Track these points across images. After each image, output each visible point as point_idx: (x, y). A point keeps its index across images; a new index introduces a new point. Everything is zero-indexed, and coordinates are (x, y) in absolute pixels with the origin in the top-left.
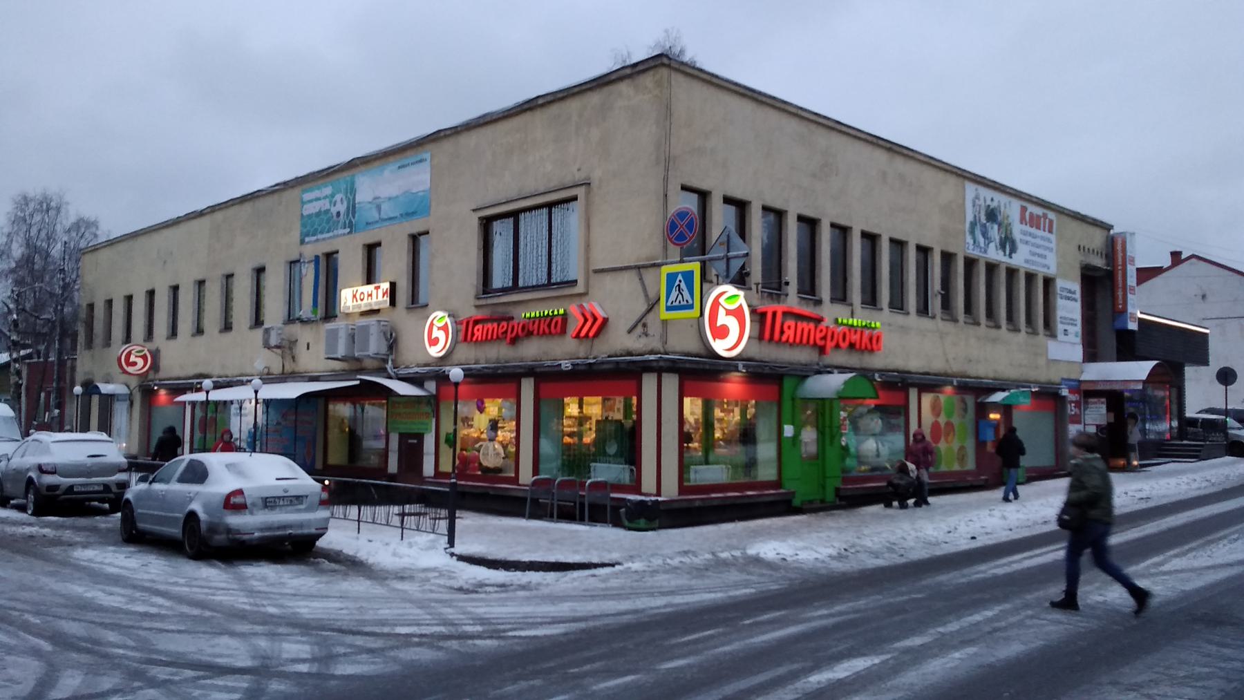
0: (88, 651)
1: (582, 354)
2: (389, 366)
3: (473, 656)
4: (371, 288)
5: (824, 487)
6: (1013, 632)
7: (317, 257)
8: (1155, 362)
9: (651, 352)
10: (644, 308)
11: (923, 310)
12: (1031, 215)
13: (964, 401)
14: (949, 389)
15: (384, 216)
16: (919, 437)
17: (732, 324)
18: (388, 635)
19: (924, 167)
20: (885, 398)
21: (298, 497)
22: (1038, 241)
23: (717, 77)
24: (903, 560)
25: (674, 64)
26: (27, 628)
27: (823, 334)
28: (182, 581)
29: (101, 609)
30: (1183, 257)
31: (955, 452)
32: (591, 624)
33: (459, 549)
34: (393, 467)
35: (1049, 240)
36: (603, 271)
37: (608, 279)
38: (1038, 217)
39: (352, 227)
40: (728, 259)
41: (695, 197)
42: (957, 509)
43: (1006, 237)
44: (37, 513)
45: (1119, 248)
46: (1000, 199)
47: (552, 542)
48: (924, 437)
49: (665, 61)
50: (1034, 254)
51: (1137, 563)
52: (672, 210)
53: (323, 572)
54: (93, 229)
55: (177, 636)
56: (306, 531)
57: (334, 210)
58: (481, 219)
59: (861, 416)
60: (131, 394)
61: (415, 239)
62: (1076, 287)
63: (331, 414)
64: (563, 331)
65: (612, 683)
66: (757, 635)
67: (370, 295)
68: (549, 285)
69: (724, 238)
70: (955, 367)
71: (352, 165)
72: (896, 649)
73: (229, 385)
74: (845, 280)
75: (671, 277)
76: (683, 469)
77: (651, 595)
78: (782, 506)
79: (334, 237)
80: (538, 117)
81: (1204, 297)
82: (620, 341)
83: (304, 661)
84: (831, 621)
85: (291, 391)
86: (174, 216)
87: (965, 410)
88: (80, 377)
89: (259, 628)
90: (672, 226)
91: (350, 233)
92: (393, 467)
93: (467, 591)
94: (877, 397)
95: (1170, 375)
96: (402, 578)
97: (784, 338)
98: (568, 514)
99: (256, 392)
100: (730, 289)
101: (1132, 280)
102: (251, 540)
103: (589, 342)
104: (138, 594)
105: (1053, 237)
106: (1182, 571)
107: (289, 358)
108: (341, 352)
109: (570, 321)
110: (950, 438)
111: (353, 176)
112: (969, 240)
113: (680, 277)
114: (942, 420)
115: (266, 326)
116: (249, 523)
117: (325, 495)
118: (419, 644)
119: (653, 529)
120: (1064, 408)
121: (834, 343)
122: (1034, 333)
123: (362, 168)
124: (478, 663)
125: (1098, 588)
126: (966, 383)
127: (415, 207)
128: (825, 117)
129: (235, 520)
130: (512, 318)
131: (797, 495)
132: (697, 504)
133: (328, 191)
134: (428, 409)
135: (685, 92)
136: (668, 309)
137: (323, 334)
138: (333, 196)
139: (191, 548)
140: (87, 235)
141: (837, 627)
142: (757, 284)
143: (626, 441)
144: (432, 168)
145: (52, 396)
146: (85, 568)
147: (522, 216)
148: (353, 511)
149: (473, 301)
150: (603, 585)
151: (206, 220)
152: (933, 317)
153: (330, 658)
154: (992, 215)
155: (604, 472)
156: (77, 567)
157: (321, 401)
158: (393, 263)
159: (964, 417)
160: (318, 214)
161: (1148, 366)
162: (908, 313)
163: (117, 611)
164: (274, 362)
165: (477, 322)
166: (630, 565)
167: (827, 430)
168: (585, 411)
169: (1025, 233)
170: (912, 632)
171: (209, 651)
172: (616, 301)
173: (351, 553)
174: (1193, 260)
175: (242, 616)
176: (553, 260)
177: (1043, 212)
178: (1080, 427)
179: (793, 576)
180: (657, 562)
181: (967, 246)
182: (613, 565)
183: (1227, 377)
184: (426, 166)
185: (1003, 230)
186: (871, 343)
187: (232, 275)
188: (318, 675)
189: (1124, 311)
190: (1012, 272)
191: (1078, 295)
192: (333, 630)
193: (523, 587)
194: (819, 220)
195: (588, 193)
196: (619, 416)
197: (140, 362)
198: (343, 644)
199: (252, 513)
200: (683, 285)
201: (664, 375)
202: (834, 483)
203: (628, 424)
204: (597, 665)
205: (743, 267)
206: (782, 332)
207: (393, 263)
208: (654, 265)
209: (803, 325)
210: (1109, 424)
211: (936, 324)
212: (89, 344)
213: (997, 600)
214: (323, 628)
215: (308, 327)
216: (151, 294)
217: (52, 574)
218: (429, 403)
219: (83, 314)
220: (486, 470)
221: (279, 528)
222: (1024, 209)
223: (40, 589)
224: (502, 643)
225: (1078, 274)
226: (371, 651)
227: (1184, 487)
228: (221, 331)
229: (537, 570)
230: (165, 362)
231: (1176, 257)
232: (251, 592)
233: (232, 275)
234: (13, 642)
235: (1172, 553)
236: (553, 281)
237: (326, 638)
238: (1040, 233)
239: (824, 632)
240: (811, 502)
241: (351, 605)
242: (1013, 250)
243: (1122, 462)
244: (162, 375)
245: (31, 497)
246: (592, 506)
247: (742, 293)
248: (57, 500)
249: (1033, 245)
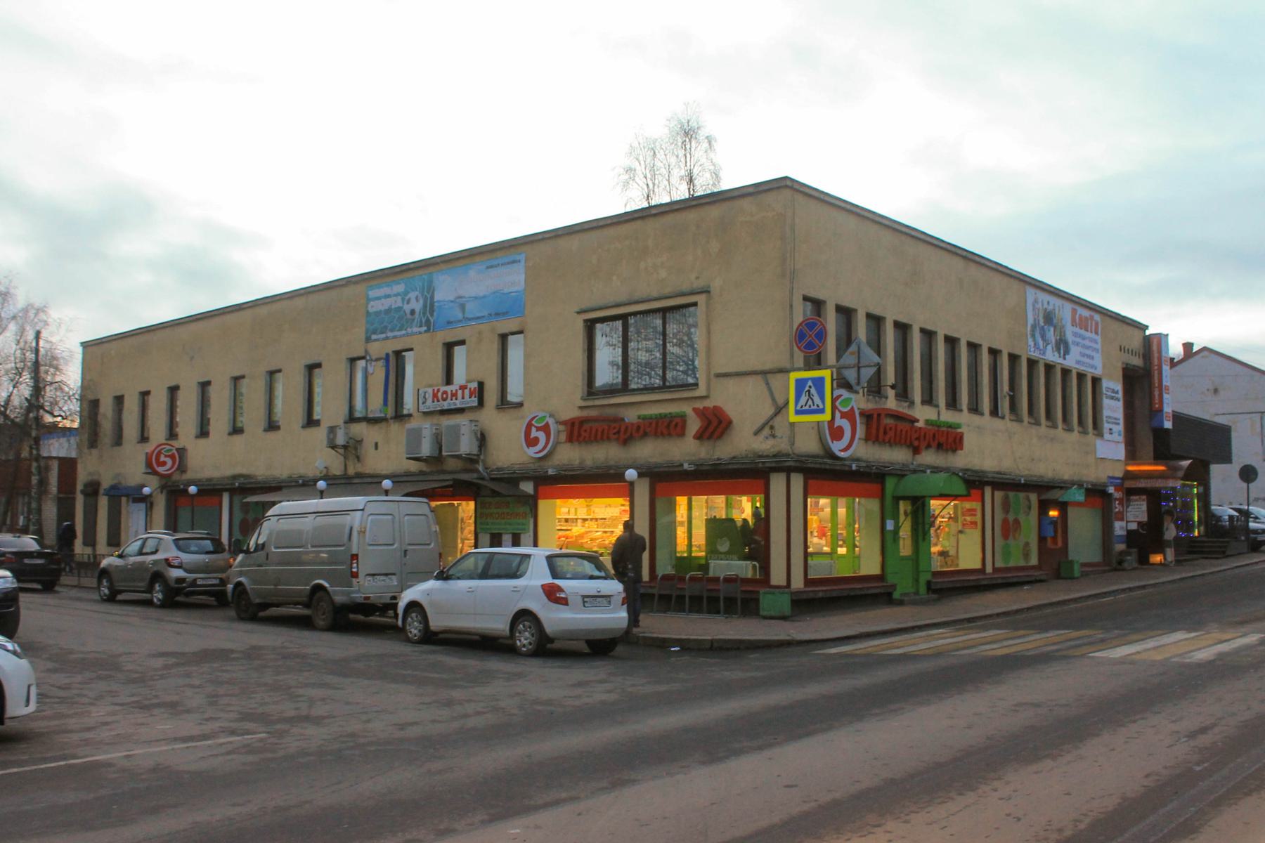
5: (917, 581)
7: (387, 355)
10: (771, 411)
11: (995, 412)
22: (1087, 343)
35: (1096, 342)
37: (731, 383)
39: (429, 326)
45: (1155, 348)
46: (1056, 302)
49: (789, 183)
50: (1083, 355)
57: (407, 308)
58: (586, 321)
62: (1119, 387)
74: (931, 382)
75: (800, 384)
79: (407, 335)
81: (1216, 391)
82: (744, 442)
105: (1099, 338)
112: (1031, 343)
113: (810, 383)
122: (1055, 427)
127: (504, 307)
131: (898, 588)
132: (820, 595)
133: (400, 288)
136: (798, 412)
138: (406, 293)
152: (1003, 418)
154: (1049, 318)
160: (388, 311)
169: (1075, 334)
172: (744, 405)
174: (1206, 353)
178: (1123, 524)
183: (1248, 474)
184: (520, 268)
186: (949, 440)
189: (1161, 410)
190: (1066, 372)
191: (1120, 395)
200: (813, 391)
206: (885, 433)
222: (1074, 311)
225: (1120, 374)
238: (1088, 334)
242: (1067, 352)
244: (189, 475)
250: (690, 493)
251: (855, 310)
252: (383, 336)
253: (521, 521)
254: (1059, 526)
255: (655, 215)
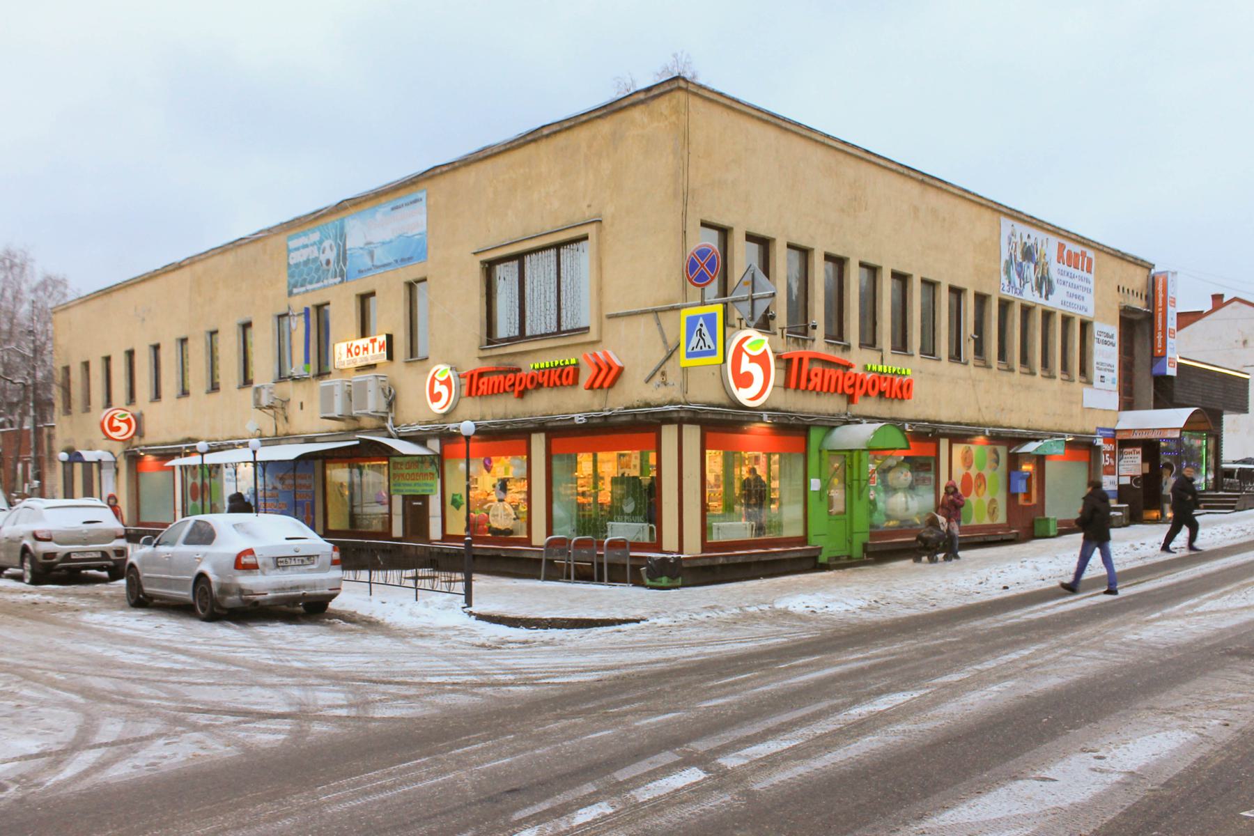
0: (123, 703)
1: (596, 407)
2: (389, 424)
3: (510, 700)
4: (365, 342)
5: (851, 542)
6: (1050, 668)
7: (307, 310)
8: (1192, 410)
9: (671, 403)
10: (663, 355)
11: (956, 356)
12: (1069, 252)
13: (995, 452)
14: (981, 438)
15: (377, 263)
16: (952, 490)
17: (757, 371)
18: (421, 684)
19: (957, 201)
20: (916, 450)
21: (309, 557)
22: (1076, 282)
23: (738, 102)
24: (935, 610)
25: (691, 88)
26: (54, 684)
27: (850, 383)
28: (200, 640)
29: (122, 666)
30: (1225, 300)
31: (985, 506)
32: (624, 672)
33: (477, 608)
34: (397, 530)
35: (1088, 281)
36: (617, 316)
37: (622, 324)
38: (1076, 255)
39: (343, 276)
40: (753, 300)
41: (715, 233)
42: (988, 561)
43: (1043, 277)
44: (36, 581)
45: (1160, 288)
46: (1037, 235)
47: (572, 601)
48: (956, 490)
49: (682, 84)
50: (1071, 295)
51: (1171, 606)
52: (692, 247)
53: (340, 631)
54: (61, 288)
55: (208, 688)
56: (319, 592)
57: (323, 258)
58: (483, 262)
59: (890, 469)
60: (116, 462)
61: (411, 286)
62: (1114, 330)
63: (328, 479)
64: (575, 382)
65: (653, 720)
66: (795, 676)
67: (366, 349)
68: (559, 333)
69: (748, 277)
70: (988, 416)
71: (341, 207)
72: (935, 685)
73: (219, 449)
75: (692, 321)
76: (705, 529)
77: (682, 646)
78: (810, 563)
80: (544, 147)
81: (1245, 342)
82: (635, 392)
83: (341, 706)
84: (868, 663)
85: (289, 452)
86: (150, 268)
87: (997, 462)
88: (59, 443)
89: (289, 680)
90: (693, 266)
91: (342, 282)
92: (397, 530)
93: (490, 648)
94: (908, 448)
95: (1208, 423)
96: (422, 636)
97: (811, 386)
98: (584, 576)
99: (254, 452)
100: (754, 334)
101: (1172, 323)
102: (265, 600)
103: (604, 391)
104: (159, 653)
105: (1091, 277)
106: (1217, 611)
107: (281, 419)
108: (338, 410)
109: (582, 371)
110: (980, 491)
111: (342, 220)
112: (1004, 280)
113: (701, 321)
114: (973, 472)
115: (256, 385)
116: (263, 584)
117: (336, 555)
118: (453, 691)
119: (676, 587)
120: (1098, 459)
121: (863, 391)
122: (1071, 380)
123: (353, 210)
124: (516, 706)
125: (1133, 628)
126: (998, 433)
128: (853, 146)
129: (246, 580)
130: (519, 370)
132: (721, 561)
133: (315, 237)
134: (432, 469)
135: (704, 118)
136: (689, 355)
137: (317, 396)
138: (321, 242)
139: (203, 609)
140: (55, 294)
141: (873, 668)
142: (782, 329)
143: (645, 499)
144: (428, 206)
145: (30, 466)
146: (98, 631)
147: (527, 259)
148: (364, 575)
149: (476, 353)
150: (630, 639)
151: (185, 274)
152: (966, 364)
153: (367, 704)
154: (1028, 253)
155: (620, 530)
156: (89, 630)
157: (318, 463)
158: (389, 316)
159: (995, 469)
160: (306, 263)
161: (1186, 413)
162: (940, 360)
163: (140, 668)
164: (267, 424)
165: (481, 375)
166: (656, 620)
167: (855, 483)
168: (597, 471)
169: (1061, 273)
170: (949, 670)
171: (244, 699)
172: (633, 348)
173: (366, 614)
174: (1236, 304)
175: (269, 670)
176: (563, 306)
177: (1083, 250)
178: (1114, 478)
179: (824, 626)
180: (683, 617)
181: (1000, 288)
182: (637, 621)
185: (1039, 270)
187: (215, 332)
188: (358, 718)
189: (1164, 356)
190: (1047, 315)
191: (1116, 340)
192: (364, 681)
193: (546, 643)
194: (848, 259)
195: (599, 232)
196: (635, 472)
197: (124, 427)
198: (377, 692)
199: (263, 573)
200: (704, 330)
201: (685, 427)
202: (861, 538)
203: (646, 480)
204: (636, 705)
205: (767, 311)
206: (809, 380)
207: (389, 316)
208: (673, 309)
209: (830, 371)
210: (1144, 475)
211: (969, 371)
212: (68, 409)
213: (1032, 641)
214: (354, 680)
215: (300, 385)
216: (131, 354)
217: (67, 636)
218: (433, 462)
219: (59, 378)
220: (496, 532)
221: (292, 588)
223: (57, 649)
224: (537, 689)
226: (406, 697)
227: (1219, 537)
228: (208, 392)
229: (560, 627)
230: (149, 426)
231: (1218, 300)
232: (272, 650)
233: (215, 332)
234: (43, 696)
235: (1206, 596)
236: (563, 328)
237: (358, 688)
238: (1078, 272)
239: (862, 672)
240: (837, 558)
241: (376, 659)
242: (1050, 291)
243: (1155, 514)
244: (148, 439)
245: (27, 565)
246: (610, 566)
247: (766, 338)
248: (53, 570)
249: (1071, 285)
250: (594, 451)
251: (911, 276)
252: (303, 289)
253: (429, 482)
254: (1034, 482)
255: (547, 136)
